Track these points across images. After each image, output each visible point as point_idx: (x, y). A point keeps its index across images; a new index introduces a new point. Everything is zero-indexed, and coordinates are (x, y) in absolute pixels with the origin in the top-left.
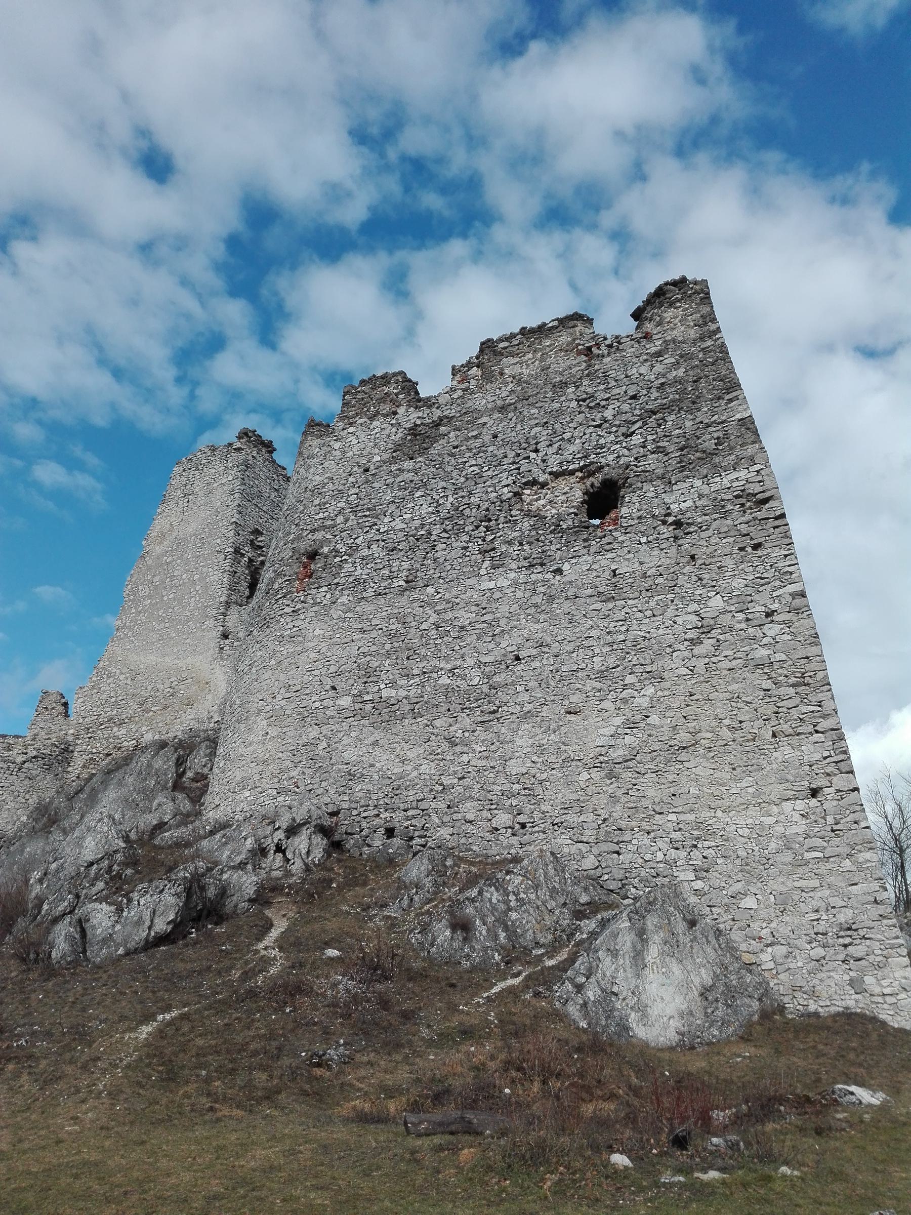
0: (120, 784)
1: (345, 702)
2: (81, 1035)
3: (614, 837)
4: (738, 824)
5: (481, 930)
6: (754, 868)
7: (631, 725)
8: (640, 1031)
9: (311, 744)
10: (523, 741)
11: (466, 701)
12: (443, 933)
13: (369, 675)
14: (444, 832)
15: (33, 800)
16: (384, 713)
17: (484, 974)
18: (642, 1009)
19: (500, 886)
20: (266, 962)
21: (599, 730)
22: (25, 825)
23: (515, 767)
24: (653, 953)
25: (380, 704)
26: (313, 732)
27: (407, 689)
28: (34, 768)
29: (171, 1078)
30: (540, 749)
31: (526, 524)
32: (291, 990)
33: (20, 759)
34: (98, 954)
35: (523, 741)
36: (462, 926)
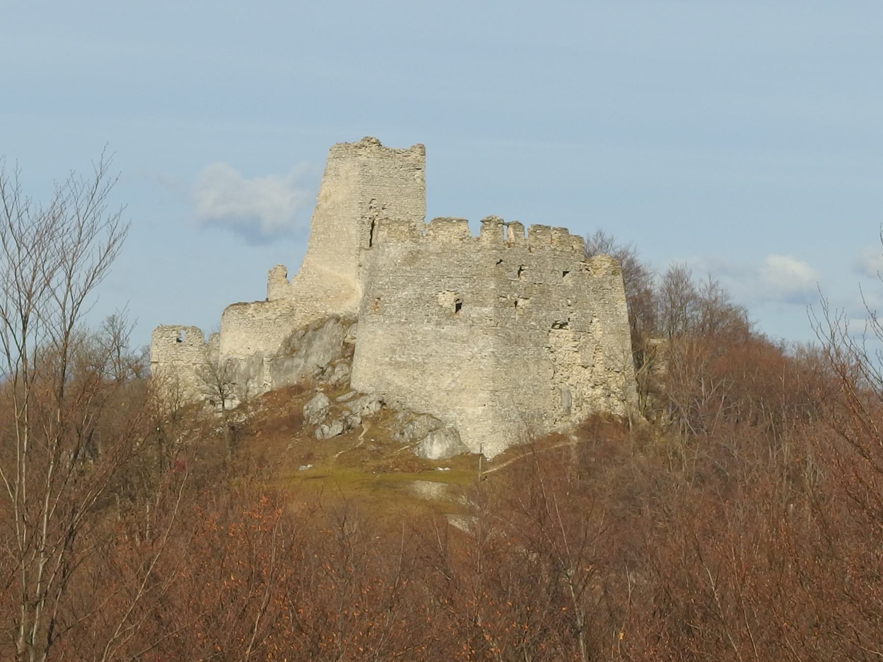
0: (321, 338)
1: (387, 359)
2: (326, 456)
3: (446, 410)
4: (470, 410)
5: (406, 434)
6: (470, 421)
7: (453, 381)
8: (429, 457)
9: (378, 372)
10: (430, 381)
11: (416, 365)
12: (398, 435)
13: (394, 351)
14: (410, 404)
15: (282, 337)
16: (397, 366)
17: (404, 444)
18: (431, 453)
19: (413, 425)
20: (359, 441)
21: (446, 382)
22: (280, 348)
23: (428, 388)
24: (435, 442)
25: (397, 362)
26: (378, 367)
27: (403, 359)
28: (280, 321)
29: (341, 463)
30: (433, 384)
31: (437, 309)
32: (362, 448)
33: (274, 317)
34: (327, 437)
35: (430, 381)
36: (402, 434)
